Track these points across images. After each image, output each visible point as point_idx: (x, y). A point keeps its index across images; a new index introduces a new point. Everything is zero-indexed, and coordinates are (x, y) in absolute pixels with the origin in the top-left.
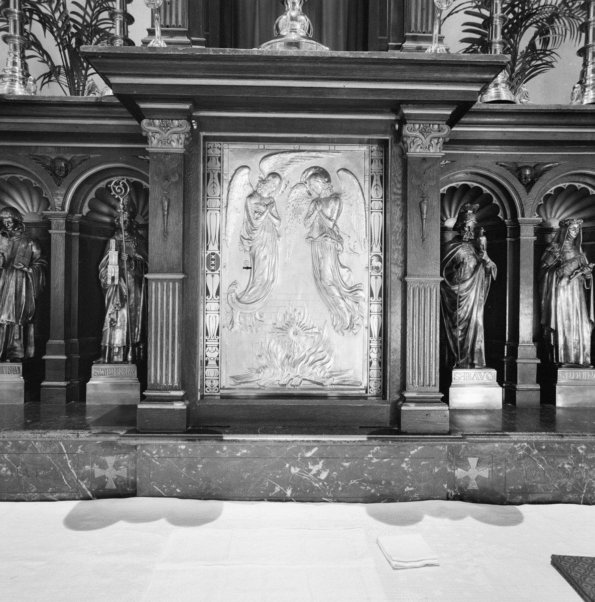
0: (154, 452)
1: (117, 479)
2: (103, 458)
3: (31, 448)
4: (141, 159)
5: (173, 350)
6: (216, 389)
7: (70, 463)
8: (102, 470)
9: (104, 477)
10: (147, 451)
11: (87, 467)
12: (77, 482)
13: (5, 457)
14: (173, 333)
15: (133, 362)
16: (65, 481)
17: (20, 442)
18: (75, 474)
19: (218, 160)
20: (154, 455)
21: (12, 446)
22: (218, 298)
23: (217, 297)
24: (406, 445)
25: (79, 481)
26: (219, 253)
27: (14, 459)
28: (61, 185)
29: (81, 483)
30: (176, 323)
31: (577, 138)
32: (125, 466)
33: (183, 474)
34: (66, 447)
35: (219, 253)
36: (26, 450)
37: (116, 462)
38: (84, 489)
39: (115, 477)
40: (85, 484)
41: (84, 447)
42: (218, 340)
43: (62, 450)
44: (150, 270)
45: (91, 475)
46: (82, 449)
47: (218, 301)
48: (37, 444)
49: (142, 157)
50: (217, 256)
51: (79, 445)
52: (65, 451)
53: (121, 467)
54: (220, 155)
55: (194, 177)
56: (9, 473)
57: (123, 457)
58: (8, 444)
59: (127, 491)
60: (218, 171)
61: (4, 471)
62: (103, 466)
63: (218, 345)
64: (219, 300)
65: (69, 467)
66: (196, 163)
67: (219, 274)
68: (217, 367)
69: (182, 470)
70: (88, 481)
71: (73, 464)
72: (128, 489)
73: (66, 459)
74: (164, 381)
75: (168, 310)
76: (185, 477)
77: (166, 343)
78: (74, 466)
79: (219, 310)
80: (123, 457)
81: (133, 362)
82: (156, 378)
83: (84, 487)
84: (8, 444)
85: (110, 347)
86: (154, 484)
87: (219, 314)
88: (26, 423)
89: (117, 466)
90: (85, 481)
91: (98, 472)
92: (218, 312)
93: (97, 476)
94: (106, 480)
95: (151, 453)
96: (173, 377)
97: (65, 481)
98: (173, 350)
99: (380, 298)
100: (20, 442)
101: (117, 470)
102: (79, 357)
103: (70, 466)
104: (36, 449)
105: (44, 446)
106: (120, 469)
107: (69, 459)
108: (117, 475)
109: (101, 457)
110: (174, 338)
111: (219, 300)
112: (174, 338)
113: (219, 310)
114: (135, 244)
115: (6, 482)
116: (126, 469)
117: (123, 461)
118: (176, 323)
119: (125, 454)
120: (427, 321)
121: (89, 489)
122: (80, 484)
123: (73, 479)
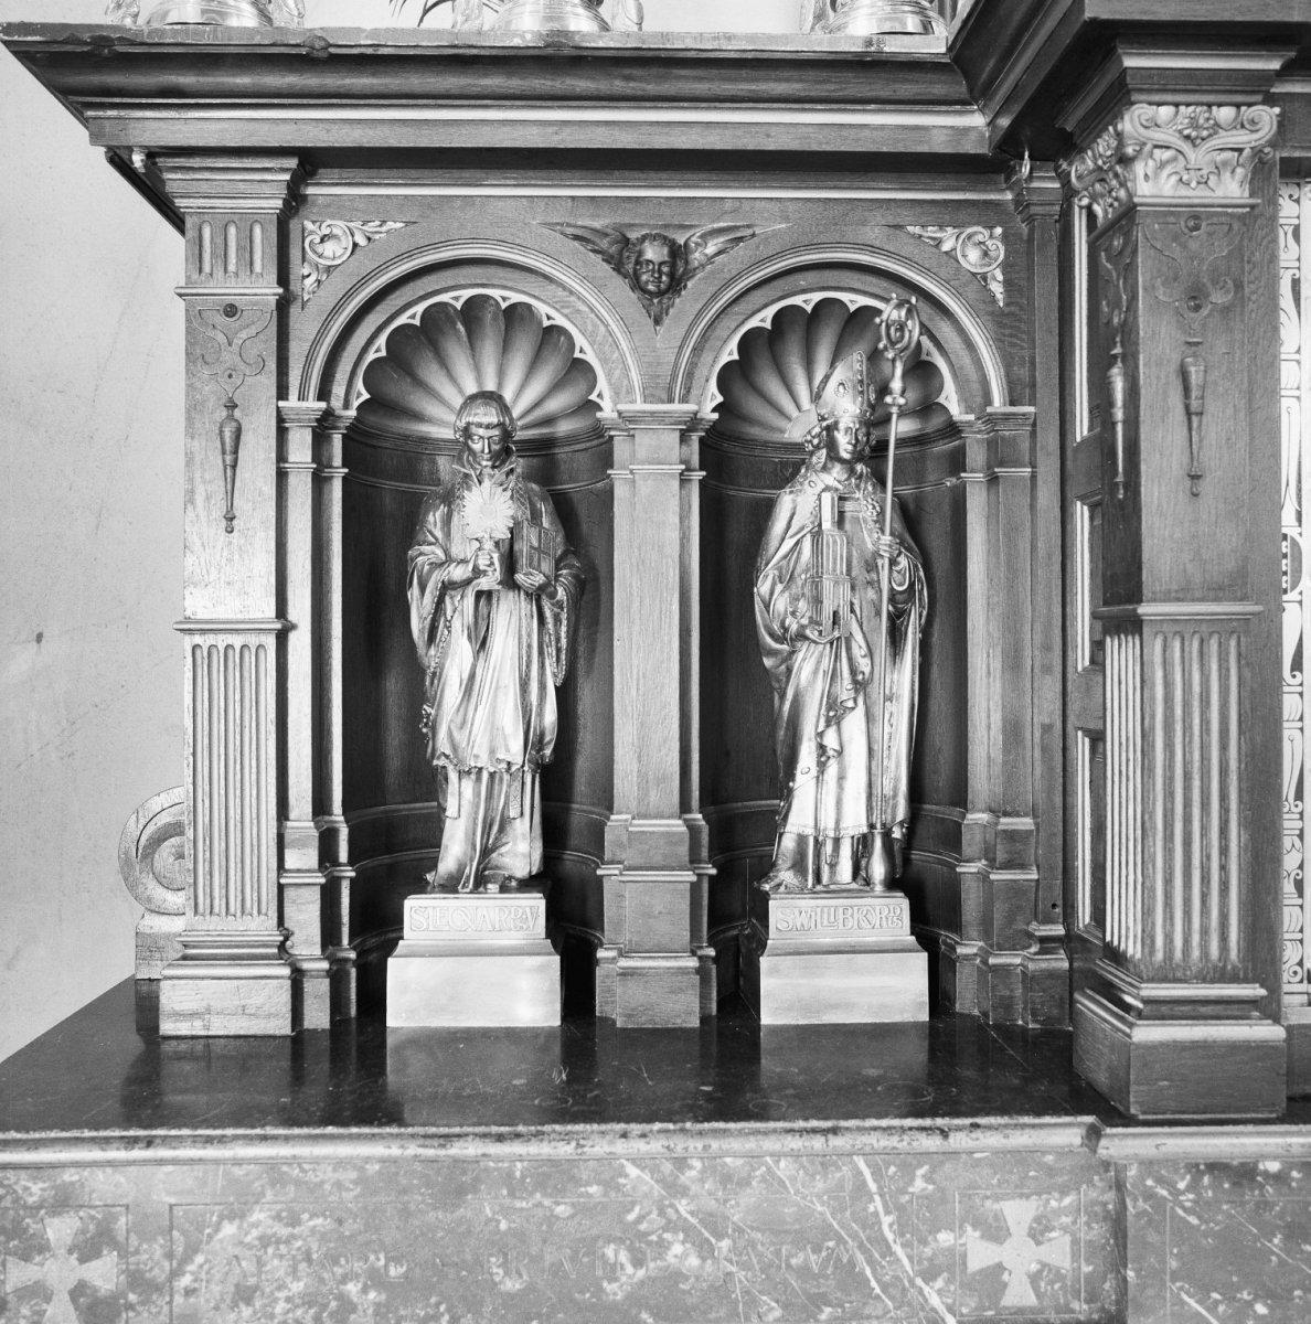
0: (1182, 1185)
1: (1040, 1272)
2: (996, 1206)
3: (763, 1180)
4: (913, 236)
5: (1224, 851)
6: (1295, 973)
7: (891, 1225)
8: (992, 1246)
9: (1000, 1267)
10: (1160, 1181)
11: (945, 1238)
12: (912, 1282)
13: (681, 1209)
14: (1224, 797)
15: (892, 884)
16: (873, 1284)
17: (728, 1160)
18: (905, 1261)
19: (1290, 235)
20: (1183, 1193)
21: (703, 1171)
22: (1298, 680)
23: (1294, 676)
24: (577, 1133)
25: (919, 1281)
26: (1300, 534)
27: (711, 1215)
28: (667, 321)
29: (926, 1289)
30: (1233, 765)
31: (750, 143)
32: (1064, 1229)
33: (1273, 1253)
34: (877, 1174)
35: (1300, 534)
36: (748, 1184)
37: (1037, 1219)
38: (933, 1310)
39: (1034, 1267)
40: (940, 1292)
41: (933, 1170)
42: (1301, 814)
43: (864, 1183)
44: (1146, 592)
45: (953, 1263)
46: (928, 1179)
47: (1299, 689)
48: (783, 1164)
49: (917, 230)
50: (1295, 544)
51: (920, 1165)
52: (873, 1186)
53: (1053, 1234)
54: (1296, 222)
55: (1260, 291)
56: (694, 1261)
57: (1060, 1200)
58: (691, 1168)
59: (1073, 1311)
60: (1291, 272)
61: (676, 1256)
62: (996, 1232)
63: (1302, 830)
64: (1301, 685)
65: (886, 1240)
66: (1267, 248)
67: (1300, 602)
68: (1299, 901)
69: (1270, 1241)
70: (949, 1281)
71: (902, 1228)
72: (1075, 1305)
73: (876, 1214)
74: (1196, 953)
75: (1205, 723)
76: (1282, 1263)
77: (1202, 828)
78: (902, 1235)
79: (1301, 719)
80: (1060, 1200)
81: (892, 884)
82: (1169, 938)
83: (935, 1301)
84: (691, 1168)
85: (816, 840)
86: (1181, 1288)
87: (1302, 729)
88: (916, 1093)
89: (1039, 1231)
90: (939, 1283)
91: (980, 1254)
92: (1299, 724)
93: (974, 1264)
94: (1005, 1277)
95: (1171, 1186)
96: (1224, 938)
97: (873, 1284)
98: (1224, 851)
99: (1297, 673)
100: (728, 1160)
101: (1038, 1243)
102: (713, 871)
103: (890, 1236)
104: (781, 1183)
105: (806, 1173)
106: (1050, 1240)
107: (888, 1213)
108: (1040, 1262)
109: (988, 1203)
110: (1224, 809)
111: (1301, 685)
112: (1224, 809)
113: (1301, 719)
114: (874, 508)
115: (684, 1292)
116: (1068, 1238)
117: (1058, 1212)
118: (1233, 765)
119: (1064, 1192)
120: (219, 727)
121: (950, 1309)
122: (921, 1292)
123: (897, 1278)
